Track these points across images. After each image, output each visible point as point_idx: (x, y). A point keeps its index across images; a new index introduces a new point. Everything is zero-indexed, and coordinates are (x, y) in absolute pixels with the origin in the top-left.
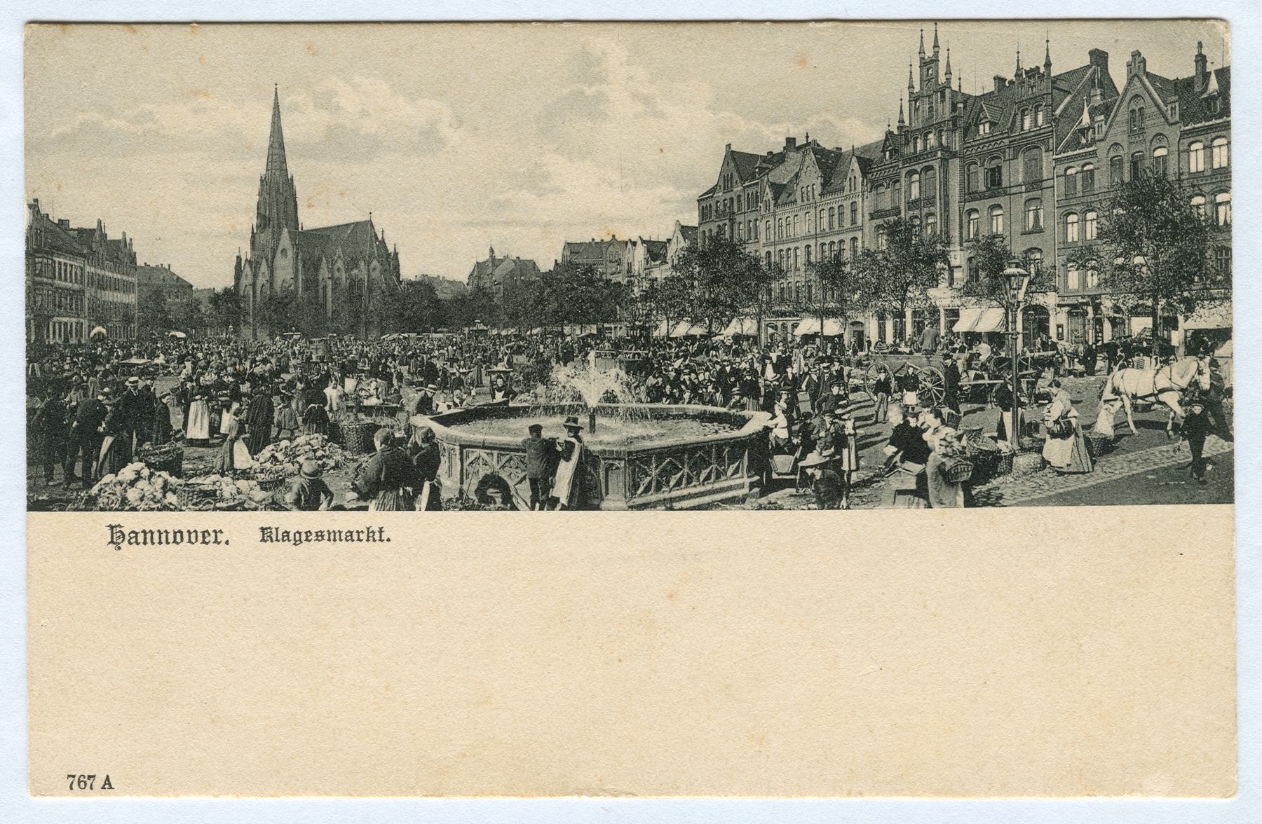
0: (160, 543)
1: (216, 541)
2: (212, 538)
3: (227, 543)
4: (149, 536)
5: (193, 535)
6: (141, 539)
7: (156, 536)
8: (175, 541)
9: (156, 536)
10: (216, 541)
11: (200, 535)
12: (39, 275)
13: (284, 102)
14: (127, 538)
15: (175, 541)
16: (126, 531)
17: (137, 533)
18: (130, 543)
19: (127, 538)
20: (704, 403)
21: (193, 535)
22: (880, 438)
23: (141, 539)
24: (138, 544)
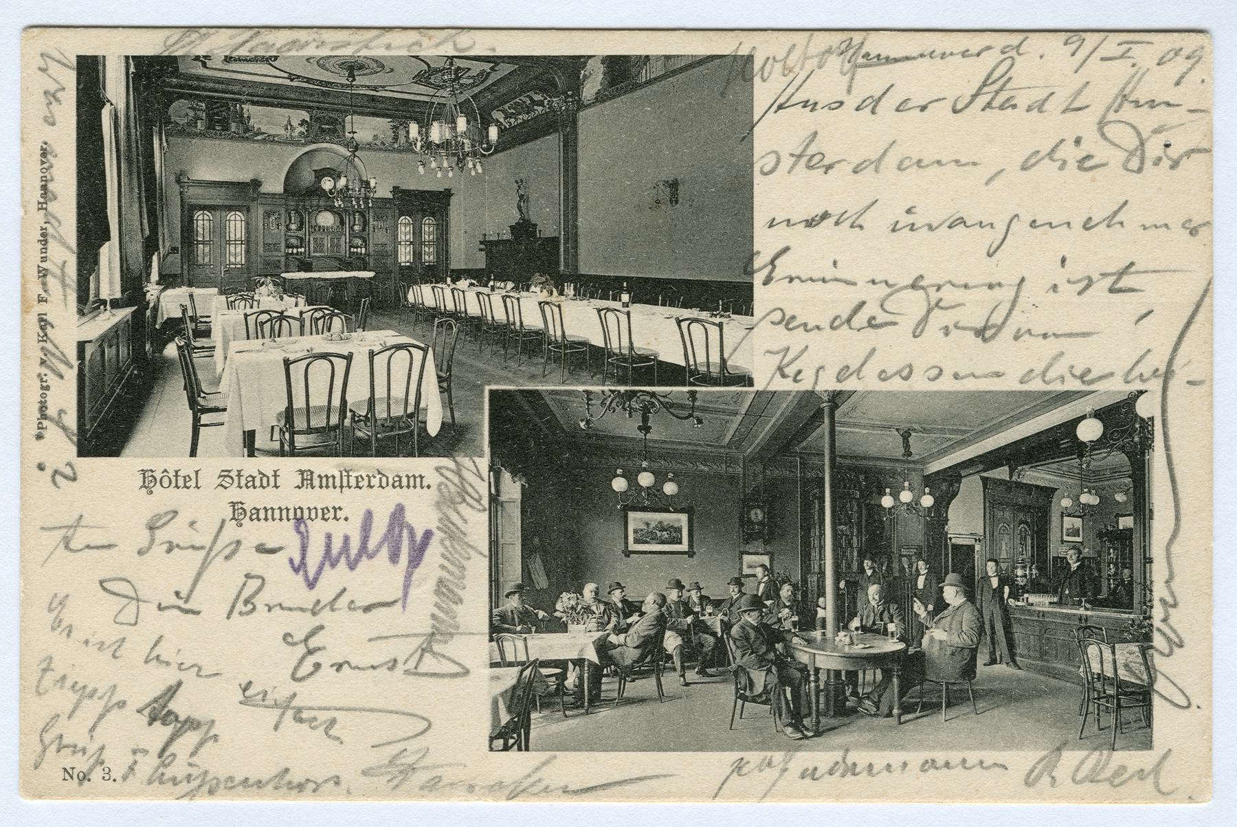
0: (281, 519)
1: (335, 518)
2: (331, 514)
3: (346, 519)
4: (270, 512)
5: (313, 512)
6: (262, 515)
7: (277, 513)
8: (262, 486)
9: (277, 513)
10: (335, 518)
11: (320, 512)
12: (400, 441)
13: (1135, 318)
14: (249, 514)
15: (262, 486)
16: (248, 507)
17: (258, 510)
18: (252, 520)
19: (249, 514)
20: (1097, 603)
21: (313, 512)
22: (1039, 156)
23: (262, 515)
24: (259, 520)
